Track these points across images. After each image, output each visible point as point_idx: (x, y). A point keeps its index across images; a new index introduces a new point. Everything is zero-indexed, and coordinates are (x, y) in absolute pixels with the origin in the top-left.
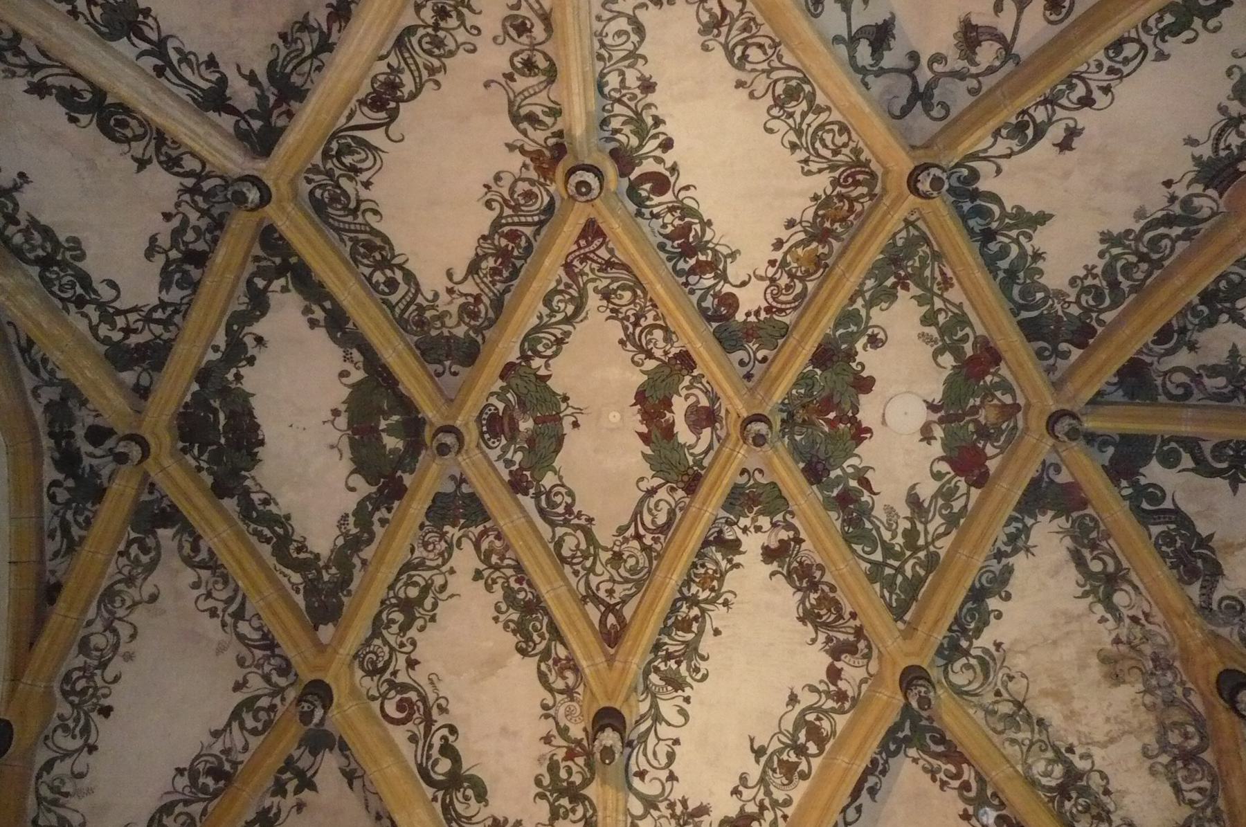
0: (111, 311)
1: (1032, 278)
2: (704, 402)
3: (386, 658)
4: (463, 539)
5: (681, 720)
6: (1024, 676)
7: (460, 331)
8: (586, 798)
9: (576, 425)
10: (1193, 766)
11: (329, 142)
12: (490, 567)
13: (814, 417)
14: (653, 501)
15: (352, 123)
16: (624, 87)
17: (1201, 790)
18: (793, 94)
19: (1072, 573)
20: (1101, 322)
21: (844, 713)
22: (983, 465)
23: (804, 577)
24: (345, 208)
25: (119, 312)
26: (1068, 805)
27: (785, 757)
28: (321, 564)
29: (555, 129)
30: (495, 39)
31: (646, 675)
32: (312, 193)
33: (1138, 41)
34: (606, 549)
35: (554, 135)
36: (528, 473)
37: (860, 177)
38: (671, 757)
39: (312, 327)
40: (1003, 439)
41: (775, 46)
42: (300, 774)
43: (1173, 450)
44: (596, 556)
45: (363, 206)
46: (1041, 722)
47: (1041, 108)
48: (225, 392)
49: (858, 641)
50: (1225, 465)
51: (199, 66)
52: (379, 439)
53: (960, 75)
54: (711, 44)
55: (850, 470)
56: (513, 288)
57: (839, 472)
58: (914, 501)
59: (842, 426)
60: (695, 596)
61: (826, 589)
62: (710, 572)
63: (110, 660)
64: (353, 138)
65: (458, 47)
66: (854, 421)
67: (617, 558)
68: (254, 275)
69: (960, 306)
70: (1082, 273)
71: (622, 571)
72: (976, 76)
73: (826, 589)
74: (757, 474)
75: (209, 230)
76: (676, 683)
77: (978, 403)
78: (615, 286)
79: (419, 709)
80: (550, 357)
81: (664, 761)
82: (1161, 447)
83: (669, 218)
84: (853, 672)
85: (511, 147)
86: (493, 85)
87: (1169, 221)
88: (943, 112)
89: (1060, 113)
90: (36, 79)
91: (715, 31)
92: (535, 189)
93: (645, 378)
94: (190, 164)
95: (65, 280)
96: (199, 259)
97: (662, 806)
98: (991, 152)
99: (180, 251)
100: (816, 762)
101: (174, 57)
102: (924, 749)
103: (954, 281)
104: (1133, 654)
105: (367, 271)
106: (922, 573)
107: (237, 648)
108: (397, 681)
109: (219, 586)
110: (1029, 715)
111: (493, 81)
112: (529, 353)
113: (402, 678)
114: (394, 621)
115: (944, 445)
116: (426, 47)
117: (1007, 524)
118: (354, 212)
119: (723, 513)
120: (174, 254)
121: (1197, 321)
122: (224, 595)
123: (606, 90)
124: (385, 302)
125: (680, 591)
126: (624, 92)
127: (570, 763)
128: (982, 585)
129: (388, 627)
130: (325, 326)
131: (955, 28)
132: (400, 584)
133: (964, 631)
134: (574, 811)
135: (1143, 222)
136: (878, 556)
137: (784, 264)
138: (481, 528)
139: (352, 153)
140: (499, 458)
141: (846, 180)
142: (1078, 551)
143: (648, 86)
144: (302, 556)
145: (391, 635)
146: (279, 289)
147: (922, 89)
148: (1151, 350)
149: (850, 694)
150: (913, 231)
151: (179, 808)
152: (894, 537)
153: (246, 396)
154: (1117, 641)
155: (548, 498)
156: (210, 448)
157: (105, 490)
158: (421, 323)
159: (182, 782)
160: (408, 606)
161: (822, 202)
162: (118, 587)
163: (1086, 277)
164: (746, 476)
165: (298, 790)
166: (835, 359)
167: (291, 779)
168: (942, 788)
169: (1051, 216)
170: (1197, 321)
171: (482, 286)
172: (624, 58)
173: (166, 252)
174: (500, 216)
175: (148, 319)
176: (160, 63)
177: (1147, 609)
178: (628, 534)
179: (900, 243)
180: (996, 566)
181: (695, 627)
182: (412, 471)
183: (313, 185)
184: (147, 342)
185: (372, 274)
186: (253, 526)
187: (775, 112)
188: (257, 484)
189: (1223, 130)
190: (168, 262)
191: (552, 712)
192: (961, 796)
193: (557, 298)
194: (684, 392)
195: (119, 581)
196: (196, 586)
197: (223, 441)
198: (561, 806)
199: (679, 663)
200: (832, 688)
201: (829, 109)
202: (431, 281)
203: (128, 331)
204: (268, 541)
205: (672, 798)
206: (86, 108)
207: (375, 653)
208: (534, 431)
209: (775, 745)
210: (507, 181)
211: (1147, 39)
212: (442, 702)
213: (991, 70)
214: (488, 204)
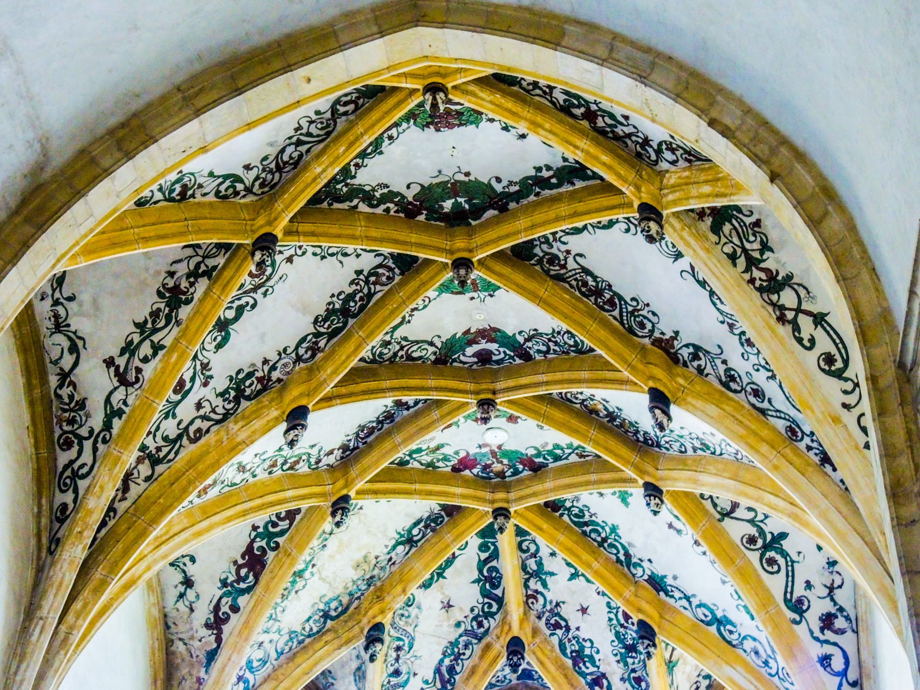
4: (383, 257)
9: (472, 298)
10: (322, 620)
12: (367, 278)
14: (426, 346)
17: (311, 629)
19: (408, 523)
20: (562, 515)
28: (349, 181)
34: (391, 337)
43: (489, 548)
52: (449, 198)
56: (573, 290)
87: (628, 555)
109: (319, 126)
138: (393, 266)
174: (626, 303)
188: (404, 131)
191: (283, 355)
192: (267, 523)
198: (229, 393)
212: (271, 290)
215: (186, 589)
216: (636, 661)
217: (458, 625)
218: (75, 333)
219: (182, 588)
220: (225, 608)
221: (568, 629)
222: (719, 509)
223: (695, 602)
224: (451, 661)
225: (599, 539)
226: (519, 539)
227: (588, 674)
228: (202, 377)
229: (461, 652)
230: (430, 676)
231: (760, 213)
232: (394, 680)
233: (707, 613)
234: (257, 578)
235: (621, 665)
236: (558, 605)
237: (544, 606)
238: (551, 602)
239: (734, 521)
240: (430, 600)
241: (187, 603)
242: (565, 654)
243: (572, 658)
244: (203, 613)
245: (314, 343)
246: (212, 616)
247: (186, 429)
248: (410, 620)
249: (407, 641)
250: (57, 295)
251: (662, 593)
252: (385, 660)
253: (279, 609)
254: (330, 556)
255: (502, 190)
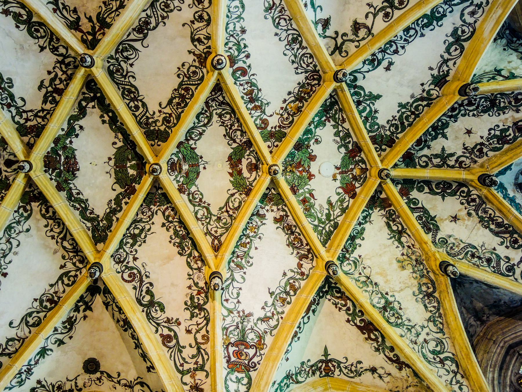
0: (21, 110)
1: (373, 120)
2: (254, 161)
3: (125, 256)
5: (242, 281)
6: (369, 267)
7: (162, 128)
8: (205, 309)
9: (205, 168)
11: (119, 46)
12: (169, 222)
13: (294, 169)
14: (233, 198)
15: (129, 38)
16: (235, 30)
17: (434, 307)
18: (294, 40)
19: (386, 231)
20: (397, 138)
21: (304, 280)
22: (354, 190)
23: (289, 230)
24: (122, 75)
25: (24, 111)
26: (386, 314)
27: (281, 296)
28: (100, 219)
29: (207, 45)
30: (189, 5)
31: (229, 263)
32: (109, 67)
33: (415, 29)
34: (214, 216)
35: (207, 48)
36: (185, 186)
37: (315, 77)
38: (238, 294)
39: (103, 124)
40: (362, 181)
41: (290, 20)
42: (86, 303)
44: (210, 218)
45: (129, 74)
46: (376, 284)
47: (380, 54)
48: (65, 148)
49: (309, 254)
50: (440, 191)
51: (70, 11)
52: (127, 170)
53: (352, 41)
54: (268, 16)
55: (307, 190)
57: (302, 191)
58: (330, 203)
59: (304, 173)
60: (248, 234)
61: (297, 234)
62: (254, 226)
63: (8, 254)
64: (128, 44)
65: (174, 8)
66: (308, 172)
67: (219, 219)
68: (81, 100)
69: (348, 130)
70: (391, 119)
71: (221, 224)
72: (358, 41)
73: (297, 234)
74: (272, 190)
75: (65, 80)
76: (240, 266)
77: (353, 167)
78: (224, 112)
79: (136, 277)
80: (197, 140)
81: (236, 296)
82: (417, 185)
83: (246, 86)
84: (306, 266)
85: (190, 52)
86: (186, 25)
87: (422, 99)
88: (346, 54)
89: (387, 56)
90: (5, 8)
91: (270, 11)
92: (197, 70)
93: (232, 150)
94: (62, 50)
95: (3, 96)
96: (61, 92)
97: (235, 312)
98: (362, 70)
99: (52, 88)
100: (293, 298)
101: (61, 6)
102: (332, 296)
103: (346, 120)
104: (408, 259)
105: (128, 102)
106: (332, 229)
107: (62, 252)
108: (129, 266)
109: (56, 227)
110: (372, 282)
111: (186, 24)
112: (189, 138)
113: (131, 264)
114: (128, 243)
115: (341, 182)
116: (162, 7)
117: (363, 212)
118: (125, 77)
119: (259, 204)
120: (50, 89)
121: (430, 138)
122: (58, 230)
123: (228, 31)
124: (134, 114)
125: (243, 232)
126: (235, 32)
127: (199, 296)
128: (354, 235)
129: (125, 245)
130: (109, 124)
131: (351, 23)
132: (132, 228)
133: (347, 251)
134: (200, 314)
135: (413, 99)
136: (316, 223)
137: (286, 109)
139: (127, 51)
140: (174, 180)
141: (310, 78)
142: (388, 222)
143: (243, 31)
144: (92, 216)
145: (127, 248)
146: (91, 107)
147: (339, 46)
148: (414, 148)
149: (306, 273)
150: (333, 100)
151: (35, 314)
152: (322, 216)
153: (74, 150)
154: (403, 254)
155: (193, 197)
156: (56, 171)
157: (11, 185)
158: (147, 124)
159: (36, 304)
160: (134, 237)
161: (302, 86)
162: (13, 225)
163: (392, 120)
164: (268, 190)
165: (84, 311)
166: (303, 147)
167: (82, 305)
168: (339, 311)
169: (381, 96)
170: (430, 138)
171: (173, 110)
172: (236, 18)
173: (47, 88)
174: (182, 81)
175: (36, 116)
176: (55, 8)
177: (413, 243)
178: (223, 210)
179: (328, 104)
180: (359, 228)
181: (248, 246)
182: (139, 184)
183: (110, 64)
184: (35, 125)
185: (129, 103)
186: (72, 203)
187: (288, 47)
188: (75, 186)
189: (442, 64)
190: (47, 92)
191: (192, 277)
192: (347, 313)
193: (202, 116)
194: (246, 157)
195: (14, 223)
196: (46, 226)
197: (62, 168)
198: (195, 312)
199: (242, 259)
200: (299, 271)
201: (306, 48)
202: (153, 107)
203: (27, 120)
204: (78, 209)
205: (239, 310)
206: (23, 22)
207: (120, 255)
208: (188, 170)
209: (278, 291)
210: (187, 66)
211: (418, 28)
213: (364, 39)
214: (178, 76)
215: (377, 373)
216: (502, 100)
217: (469, 214)
218: (135, 380)
219: (376, 375)
220: (391, 355)
221: (482, 144)
222: (366, 36)
223: (446, 56)
224: (493, 224)
225: (413, 116)
226: (418, 167)
227: (515, 135)
228: (174, 324)
229: (488, 216)
230: (499, 240)
231: (100, 2)
232: (493, 264)
233: (453, 48)
234: (377, 330)
235: (507, 111)
236: (466, 148)
237: (467, 157)
238: (464, 153)
239: (374, 27)
240: (446, 229)
241: (385, 375)
242: (501, 148)
243: (504, 143)
244: (392, 368)
245: (194, 258)
246: (395, 365)
247: (197, 343)
248: (456, 244)
249: (470, 249)
250: (115, 380)
251: (448, 79)
252: (478, 266)
253: (406, 323)
254: (386, 282)
255: (122, 143)
